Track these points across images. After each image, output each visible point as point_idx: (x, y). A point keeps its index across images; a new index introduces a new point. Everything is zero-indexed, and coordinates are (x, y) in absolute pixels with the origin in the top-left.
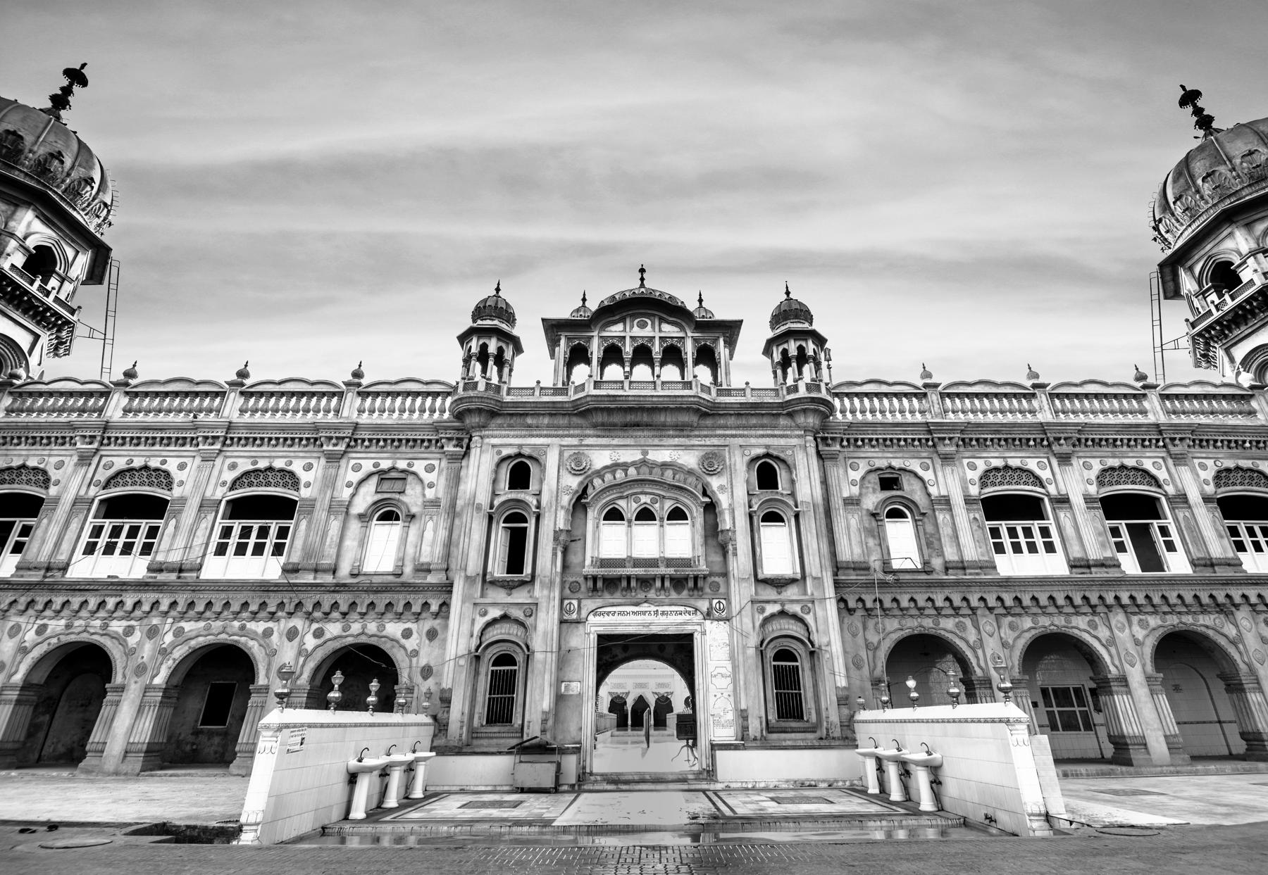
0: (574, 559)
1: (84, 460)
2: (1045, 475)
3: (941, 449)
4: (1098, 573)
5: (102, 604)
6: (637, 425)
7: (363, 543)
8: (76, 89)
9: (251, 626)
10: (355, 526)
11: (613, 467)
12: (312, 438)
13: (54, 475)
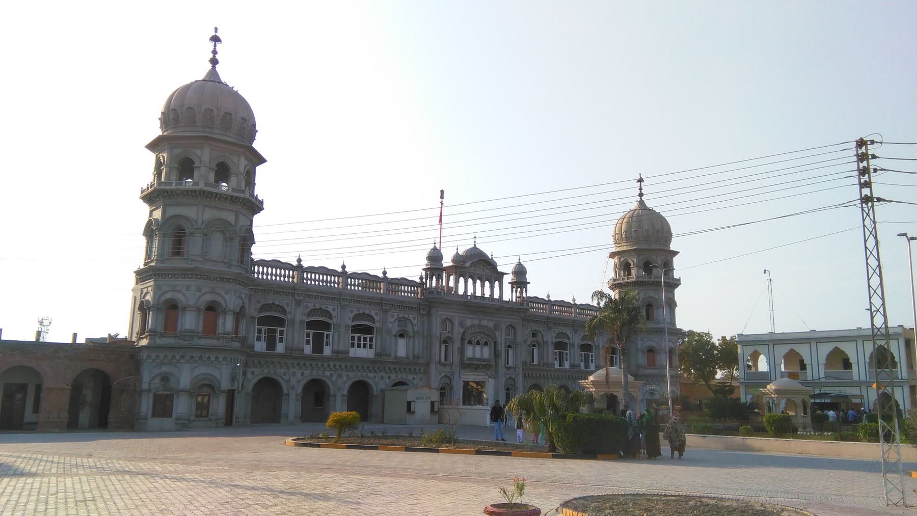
1: (298, 303)
9: (369, 374)
10: (394, 338)
13: (288, 309)
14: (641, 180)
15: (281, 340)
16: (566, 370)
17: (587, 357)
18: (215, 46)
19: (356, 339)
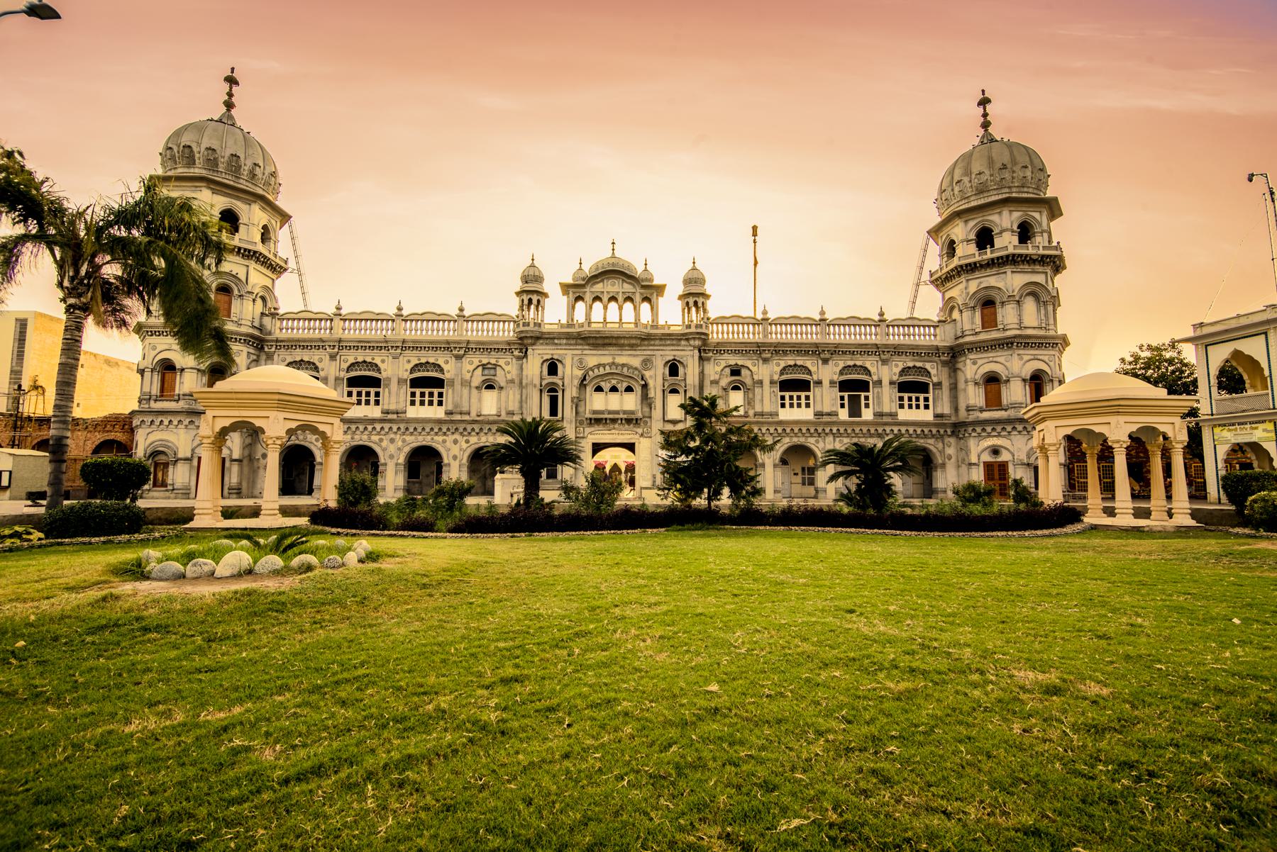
0: (581, 409)
1: (333, 357)
2: (813, 369)
3: (764, 355)
4: (826, 419)
5: (366, 429)
6: (610, 344)
7: (480, 400)
8: (235, 89)
10: (474, 392)
11: (598, 366)
12: (447, 346)
14: (984, 102)
15: (867, 406)
19: (418, 394)
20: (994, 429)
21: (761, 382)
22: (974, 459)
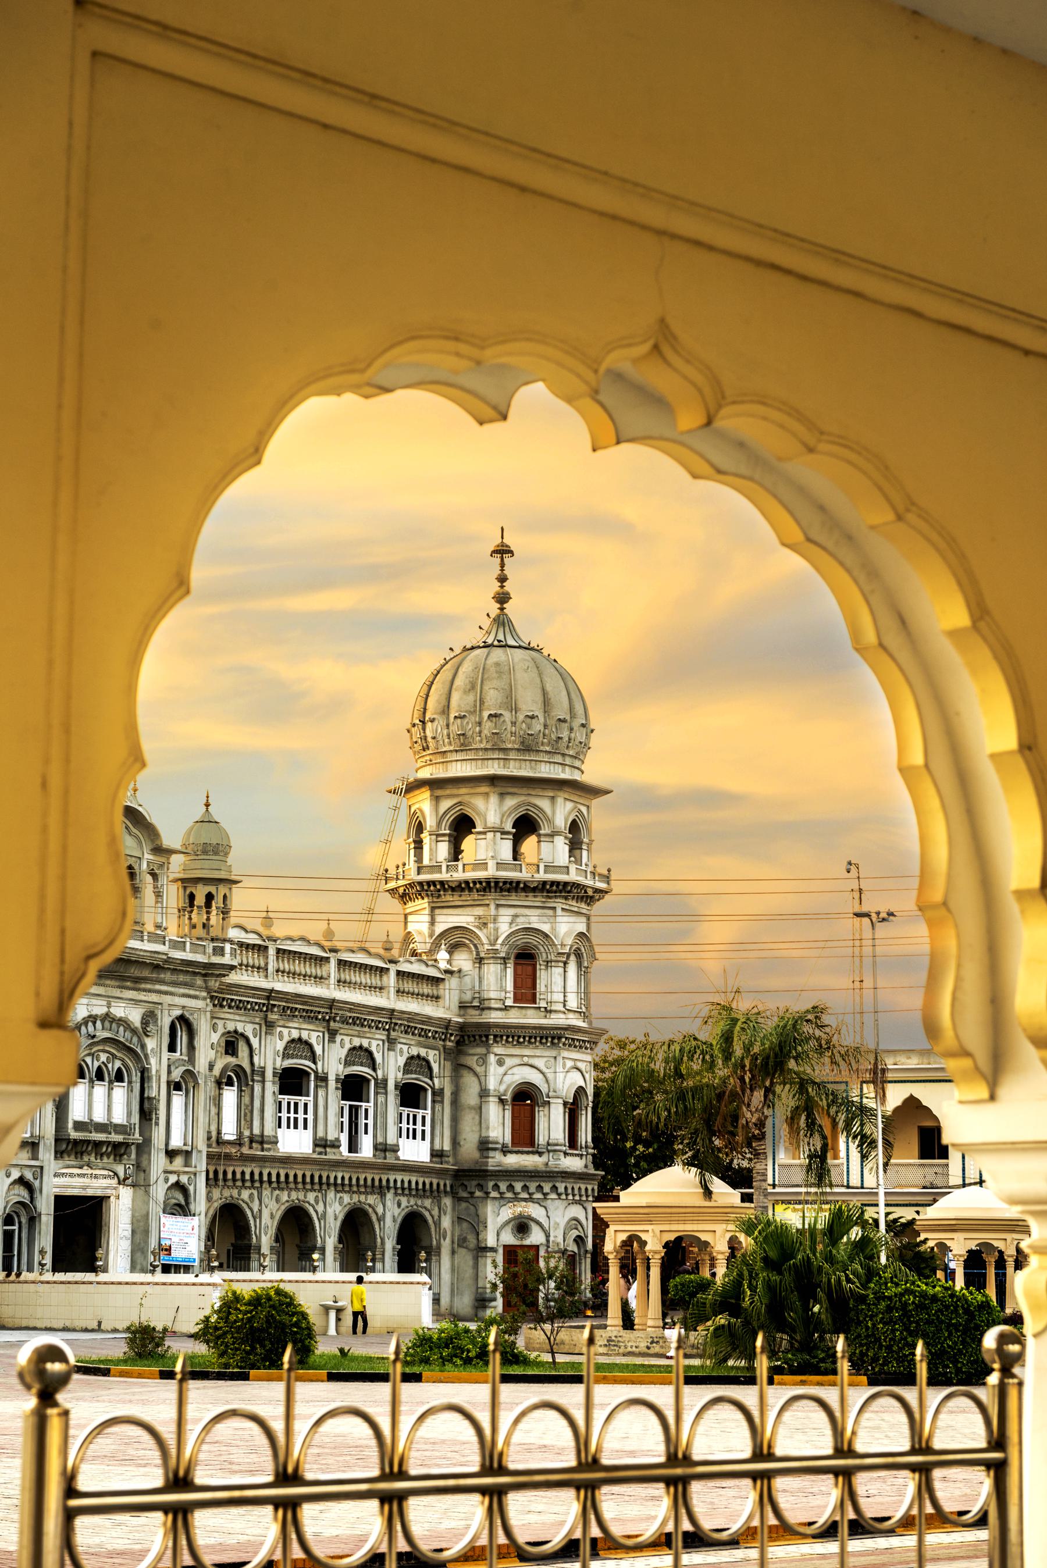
14: (503, 551)
16: (364, 1165)
17: (354, 1112)
18: (502, 565)
20: (525, 1188)
21: (262, 1073)
22: (491, 1242)
